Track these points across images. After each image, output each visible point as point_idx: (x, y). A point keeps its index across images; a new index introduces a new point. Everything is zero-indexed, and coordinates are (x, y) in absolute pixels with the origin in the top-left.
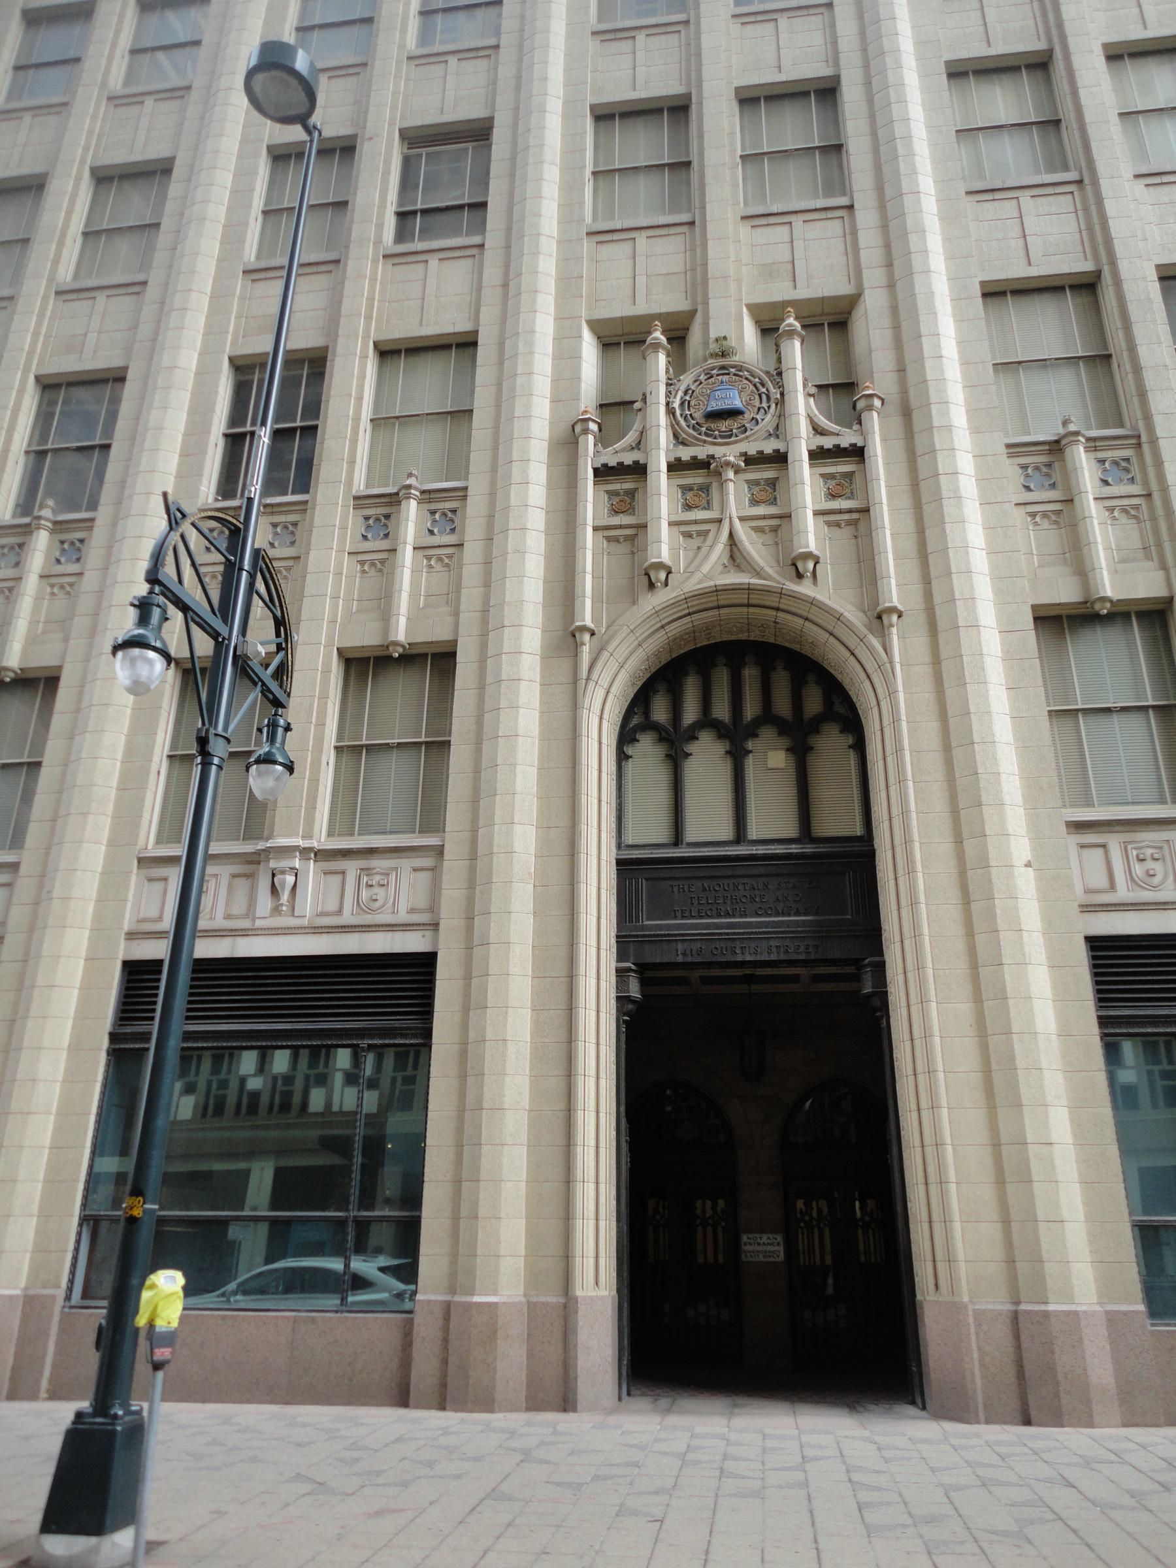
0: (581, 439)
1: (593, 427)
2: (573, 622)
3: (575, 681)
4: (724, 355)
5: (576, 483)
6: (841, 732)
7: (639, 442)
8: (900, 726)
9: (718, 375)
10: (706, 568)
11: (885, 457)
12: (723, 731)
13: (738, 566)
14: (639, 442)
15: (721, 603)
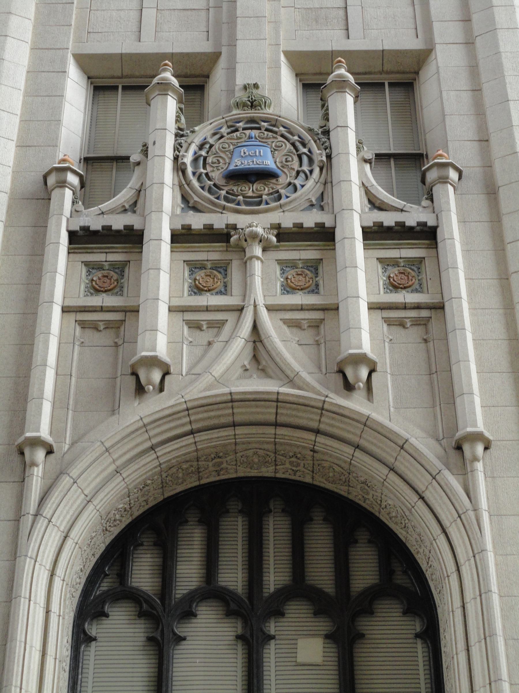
0: (55, 194)
1: (73, 179)
2: (22, 433)
3: (17, 519)
4: (253, 104)
5: (43, 250)
6: (405, 613)
7: (135, 203)
8: (489, 600)
9: (244, 129)
10: (218, 370)
11: (465, 243)
12: (233, 606)
13: (263, 370)
14: (135, 203)
15: (238, 419)
